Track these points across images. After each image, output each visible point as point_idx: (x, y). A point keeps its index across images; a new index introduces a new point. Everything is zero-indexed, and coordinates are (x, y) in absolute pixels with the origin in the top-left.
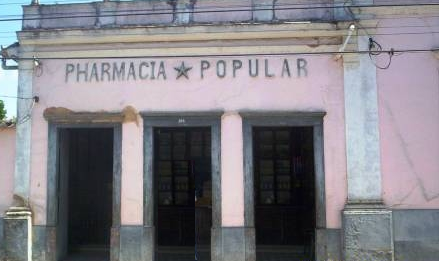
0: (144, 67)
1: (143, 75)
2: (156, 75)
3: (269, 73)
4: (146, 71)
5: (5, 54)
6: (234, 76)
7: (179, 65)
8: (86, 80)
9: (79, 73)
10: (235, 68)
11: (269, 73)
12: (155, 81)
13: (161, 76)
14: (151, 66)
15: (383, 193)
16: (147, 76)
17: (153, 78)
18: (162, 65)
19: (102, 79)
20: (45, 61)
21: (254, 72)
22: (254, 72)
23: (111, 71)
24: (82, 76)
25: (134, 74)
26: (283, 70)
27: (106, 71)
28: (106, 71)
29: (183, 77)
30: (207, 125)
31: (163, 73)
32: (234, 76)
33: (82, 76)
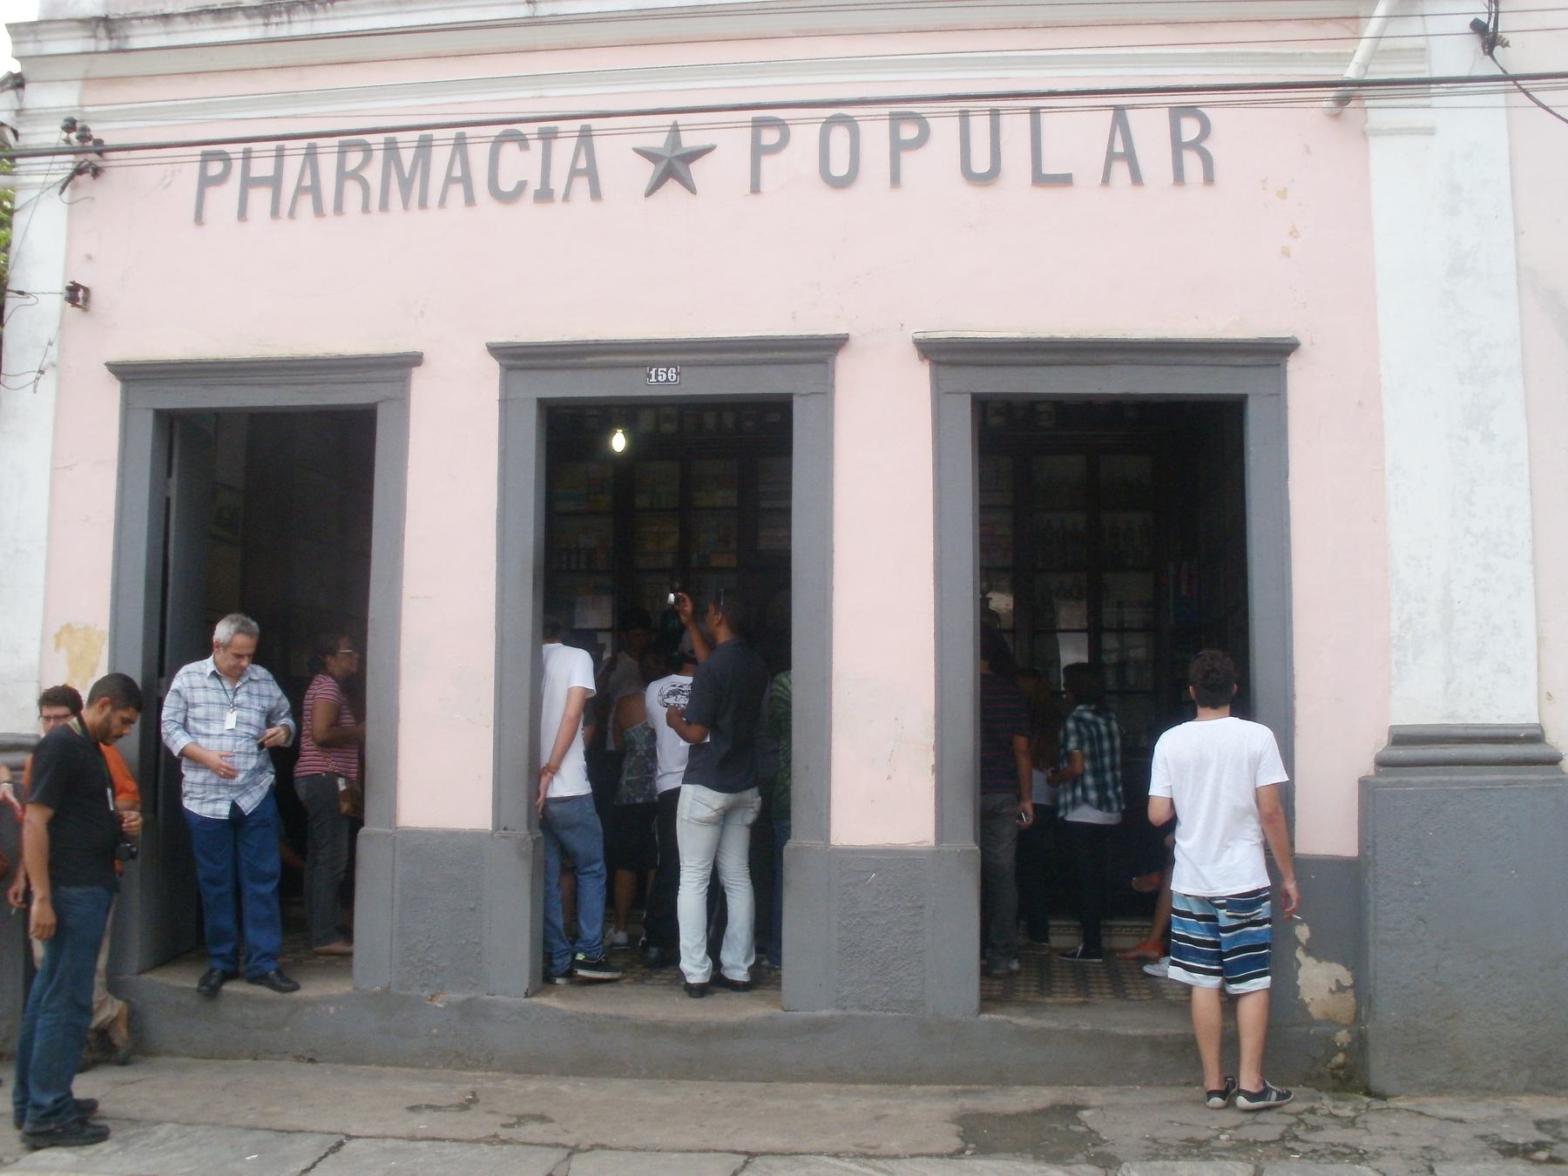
0: (509, 151)
1: (506, 185)
2: (558, 183)
3: (1048, 169)
4: (519, 165)
5: (1565, 1140)
6: (895, 179)
7: (657, 141)
8: (275, 213)
9: (248, 183)
10: (898, 147)
11: (1048, 169)
12: (556, 208)
13: (582, 184)
14: (537, 146)
15: (22, 134)
16: (522, 186)
17: (544, 195)
18: (586, 135)
19: (339, 208)
20: (110, 169)
21: (981, 164)
22: (981, 164)
23: (374, 174)
24: (260, 199)
25: (466, 180)
26: (1111, 156)
27: (356, 175)
28: (356, 175)
29: (672, 187)
30: (1393, 747)
31: (592, 174)
32: (895, 179)
33: (260, 199)
